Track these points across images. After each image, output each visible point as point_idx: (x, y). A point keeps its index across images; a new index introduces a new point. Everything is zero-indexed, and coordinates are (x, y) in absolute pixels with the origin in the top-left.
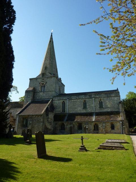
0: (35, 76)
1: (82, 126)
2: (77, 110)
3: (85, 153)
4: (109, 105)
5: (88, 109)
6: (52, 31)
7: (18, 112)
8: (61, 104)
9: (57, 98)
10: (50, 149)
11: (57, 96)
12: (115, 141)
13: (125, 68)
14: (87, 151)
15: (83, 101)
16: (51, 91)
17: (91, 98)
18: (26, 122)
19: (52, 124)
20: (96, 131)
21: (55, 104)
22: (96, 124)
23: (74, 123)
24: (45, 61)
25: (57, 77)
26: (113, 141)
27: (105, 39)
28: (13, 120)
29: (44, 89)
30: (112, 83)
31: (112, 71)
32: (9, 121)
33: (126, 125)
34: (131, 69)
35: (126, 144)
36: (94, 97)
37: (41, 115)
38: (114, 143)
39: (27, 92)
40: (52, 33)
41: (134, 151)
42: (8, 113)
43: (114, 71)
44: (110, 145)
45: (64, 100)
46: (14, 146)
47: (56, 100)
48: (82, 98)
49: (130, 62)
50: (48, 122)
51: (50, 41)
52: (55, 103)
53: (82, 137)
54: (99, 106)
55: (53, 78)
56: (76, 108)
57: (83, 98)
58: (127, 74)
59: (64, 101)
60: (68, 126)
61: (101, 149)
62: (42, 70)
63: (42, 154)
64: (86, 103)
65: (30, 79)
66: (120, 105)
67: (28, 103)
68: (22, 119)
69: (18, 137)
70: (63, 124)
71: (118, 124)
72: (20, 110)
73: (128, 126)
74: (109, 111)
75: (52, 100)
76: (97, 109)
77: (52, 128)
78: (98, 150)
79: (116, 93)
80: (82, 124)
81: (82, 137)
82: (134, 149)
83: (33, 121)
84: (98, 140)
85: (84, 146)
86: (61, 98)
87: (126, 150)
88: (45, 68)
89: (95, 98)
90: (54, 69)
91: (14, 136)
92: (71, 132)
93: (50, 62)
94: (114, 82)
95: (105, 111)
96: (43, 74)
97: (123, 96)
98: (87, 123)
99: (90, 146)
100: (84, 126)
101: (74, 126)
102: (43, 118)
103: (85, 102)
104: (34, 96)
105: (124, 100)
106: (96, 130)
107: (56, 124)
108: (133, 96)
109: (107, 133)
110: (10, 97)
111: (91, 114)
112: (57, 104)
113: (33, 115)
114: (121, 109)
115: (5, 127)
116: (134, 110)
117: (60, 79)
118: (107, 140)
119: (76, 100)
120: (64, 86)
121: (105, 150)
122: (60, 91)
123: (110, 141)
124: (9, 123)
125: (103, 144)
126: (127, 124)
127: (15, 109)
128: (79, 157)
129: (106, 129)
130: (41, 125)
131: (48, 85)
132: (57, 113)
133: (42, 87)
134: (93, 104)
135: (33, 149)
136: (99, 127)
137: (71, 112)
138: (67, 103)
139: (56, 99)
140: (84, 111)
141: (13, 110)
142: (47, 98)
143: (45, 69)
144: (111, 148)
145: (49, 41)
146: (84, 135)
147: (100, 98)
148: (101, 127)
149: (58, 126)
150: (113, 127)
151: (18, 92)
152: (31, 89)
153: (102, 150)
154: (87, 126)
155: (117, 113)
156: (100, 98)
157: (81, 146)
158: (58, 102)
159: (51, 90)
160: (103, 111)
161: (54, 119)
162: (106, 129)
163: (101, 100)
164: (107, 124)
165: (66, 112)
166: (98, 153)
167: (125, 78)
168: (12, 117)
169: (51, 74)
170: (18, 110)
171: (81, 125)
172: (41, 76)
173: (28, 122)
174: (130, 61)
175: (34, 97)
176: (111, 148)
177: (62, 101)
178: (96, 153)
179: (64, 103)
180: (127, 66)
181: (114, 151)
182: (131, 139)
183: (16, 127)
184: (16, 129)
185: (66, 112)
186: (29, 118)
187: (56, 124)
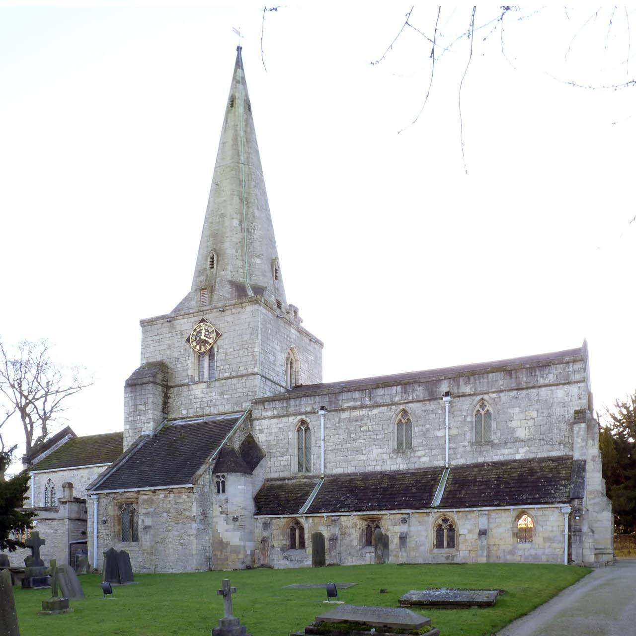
2: (363, 458)
5: (419, 454)
8: (293, 435)
9: (272, 405)
16: (242, 376)
17: (433, 397)
36: (447, 394)
40: (239, 49)
45: (306, 413)
48: (388, 401)
51: (232, 102)
54: (470, 436)
57: (397, 399)
59: (303, 422)
95: (502, 458)
112: (270, 434)
119: (364, 412)
130: (194, 532)
131: (224, 347)
132: (276, 475)
134: (441, 426)
139: (269, 414)
147: (479, 398)
160: (488, 459)
163: (483, 406)
177: (294, 420)
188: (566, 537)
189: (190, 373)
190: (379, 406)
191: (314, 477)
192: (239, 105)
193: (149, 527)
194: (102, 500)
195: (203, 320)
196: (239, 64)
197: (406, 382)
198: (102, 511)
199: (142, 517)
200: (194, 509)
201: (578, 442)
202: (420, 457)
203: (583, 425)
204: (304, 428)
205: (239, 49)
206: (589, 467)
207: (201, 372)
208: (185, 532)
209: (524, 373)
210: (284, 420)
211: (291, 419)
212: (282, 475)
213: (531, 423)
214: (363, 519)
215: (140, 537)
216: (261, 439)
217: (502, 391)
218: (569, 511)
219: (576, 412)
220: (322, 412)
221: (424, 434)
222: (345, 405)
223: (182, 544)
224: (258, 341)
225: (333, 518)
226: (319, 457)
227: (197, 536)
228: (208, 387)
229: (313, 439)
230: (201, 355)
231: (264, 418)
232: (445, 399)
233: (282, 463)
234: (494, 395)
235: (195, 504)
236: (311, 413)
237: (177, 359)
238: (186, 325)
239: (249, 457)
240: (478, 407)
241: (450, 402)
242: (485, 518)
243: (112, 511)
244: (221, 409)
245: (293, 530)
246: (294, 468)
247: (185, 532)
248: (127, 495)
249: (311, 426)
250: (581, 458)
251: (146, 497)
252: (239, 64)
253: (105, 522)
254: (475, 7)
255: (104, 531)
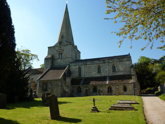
0: (53, 45)
1: (97, 89)
2: (92, 74)
3: (97, 113)
4: (121, 69)
5: (102, 73)
6: (67, 2)
7: (38, 78)
8: (77, 69)
9: (73, 63)
10: (63, 111)
11: (74, 62)
12: (126, 102)
13: (132, 32)
14: (98, 111)
15: (97, 66)
16: (68, 58)
17: (105, 63)
18: (46, 87)
19: (70, 87)
20: (109, 93)
21: (72, 70)
22: (109, 87)
23: (89, 86)
24: (61, 30)
25: (73, 45)
26: (124, 102)
27: (111, 4)
28: (35, 85)
29: (61, 56)
30: (120, 47)
31: (119, 35)
32: (31, 86)
33: (137, 87)
34: (138, 32)
35: (137, 105)
36: (107, 62)
37: (59, 80)
38: (125, 104)
39: (46, 59)
40: (67, 4)
41: (143, 111)
42: (28, 79)
43: (121, 34)
44: (121, 106)
45: (80, 65)
46: (29, 109)
47: (73, 66)
48: (96, 63)
49: (137, 25)
50: (66, 86)
51: (65, 12)
52: (71, 68)
53: (94, 99)
54: (112, 70)
55: (69, 46)
56: (91, 73)
57: (98, 63)
58: (134, 37)
59: (80, 67)
60: (84, 89)
61: (112, 109)
62: (59, 39)
63: (55, 115)
64: (100, 68)
65: (49, 48)
66: (131, 69)
67: (47, 70)
68: (42, 84)
69: (39, 100)
70: (79, 88)
71: (130, 86)
72: (40, 76)
73: (139, 88)
74: (121, 74)
75: (69, 66)
76: (110, 73)
77: (70, 92)
78: (109, 111)
79: (128, 57)
80: (97, 87)
81: (94, 99)
82: (143, 109)
83: (52, 85)
84: (111, 101)
85: (95, 108)
86: (78, 64)
87: (136, 110)
88: (62, 37)
89: (108, 63)
90: (70, 37)
91: (35, 99)
92: (87, 95)
93: (66, 31)
94: (121, 46)
95: (118, 74)
96: (60, 43)
97: (135, 60)
98: (102, 86)
99: (102, 108)
100: (98, 88)
101: (89, 89)
102: (61, 83)
103: (99, 67)
104: (52, 63)
105: (136, 64)
106: (110, 92)
107: (73, 87)
108: (144, 60)
109: (120, 94)
110: (32, 65)
111: (103, 79)
112: (73, 69)
113: (52, 80)
114: (133, 72)
115: (27, 91)
116: (145, 73)
117: (76, 46)
118: (119, 101)
119: (91, 65)
120: (80, 53)
121: (116, 111)
122: (76, 57)
123: (121, 102)
124: (30, 88)
125: (114, 105)
126: (139, 86)
127: (36, 75)
128: (90, 118)
129: (119, 91)
130: (60, 89)
131: (64, 53)
132: (74, 77)
133: (59, 54)
134: (106, 68)
135: (46, 111)
136: (113, 89)
137: (87, 76)
138: (83, 68)
139: (73, 65)
140: (98, 75)
141: (34, 76)
142: (65, 64)
143: (62, 38)
144: (121, 109)
145: (65, 12)
146: (96, 97)
147: (113, 63)
148: (115, 89)
149: (75, 89)
150: (125, 89)
151: (38, 60)
152: (50, 56)
153: (113, 111)
154: (101, 88)
155: (129, 77)
156: (113, 63)
157: (93, 108)
158: (74, 68)
159: (68, 57)
160: (116, 75)
161: (71, 83)
162: (119, 91)
163: (114, 65)
164: (120, 87)
165: (82, 77)
166: (109, 113)
167: (132, 41)
168: (34, 82)
169: (67, 42)
170: (39, 76)
171: (96, 88)
172: (58, 45)
173: (48, 87)
174: (136, 24)
175: (52, 63)
176: (121, 109)
177: (78, 67)
178: (106, 113)
179: (80, 69)
180: (134, 30)
181: (124, 111)
182: (142, 100)
183: (38, 91)
184: (37, 93)
185: (82, 77)
186: (48, 83)
187: (73, 87)
191: (82, 78)
193: (50, 88)
194: (40, 82)
200: (60, 84)
202: (102, 74)
203: (133, 68)
207: (59, 57)
210: (76, 66)
211: (77, 66)
212: (75, 77)
213: (123, 68)
217: (117, 62)
219: (131, 66)
221: (103, 70)
222: (88, 64)
224: (71, 52)
226: (83, 74)
227: (60, 90)
229: (82, 70)
231: (72, 66)
232: (107, 63)
234: (116, 63)
235: (60, 83)
236: (81, 65)
237: (55, 54)
241: (108, 64)
242: (117, 88)
244: (63, 64)
254: (131, 48)
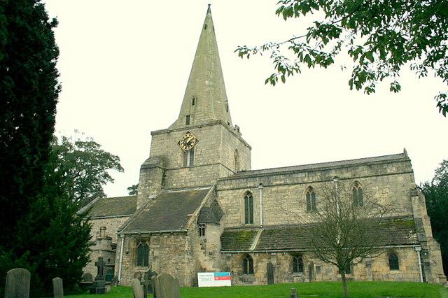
8: (242, 201)
36: (336, 177)
45: (250, 187)
48: (301, 181)
51: (205, 27)
59: (248, 193)
119: (286, 187)
132: (231, 226)
139: (227, 187)
163: (357, 185)
188: (420, 266)
189: (179, 162)
190: (295, 184)
192: (208, 27)
195: (188, 132)
196: (209, 11)
197: (309, 170)
198: (127, 245)
199: (152, 250)
200: (187, 246)
201: (415, 207)
204: (249, 197)
205: (209, 5)
206: (424, 220)
207: (185, 162)
208: (180, 260)
209: (377, 166)
211: (241, 191)
214: (291, 254)
215: (149, 263)
216: (222, 202)
218: (420, 249)
220: (261, 187)
222: (274, 183)
223: (177, 269)
225: (228, 255)
226: (259, 215)
228: (190, 170)
230: (185, 153)
231: (224, 190)
232: (335, 180)
233: (236, 218)
238: (179, 136)
239: (213, 214)
240: (308, 190)
243: (133, 245)
245: (245, 261)
246: (243, 221)
247: (180, 260)
248: (143, 236)
249: (254, 196)
250: (418, 217)
251: (155, 237)
252: (209, 11)
253: (127, 253)
255: (126, 259)
